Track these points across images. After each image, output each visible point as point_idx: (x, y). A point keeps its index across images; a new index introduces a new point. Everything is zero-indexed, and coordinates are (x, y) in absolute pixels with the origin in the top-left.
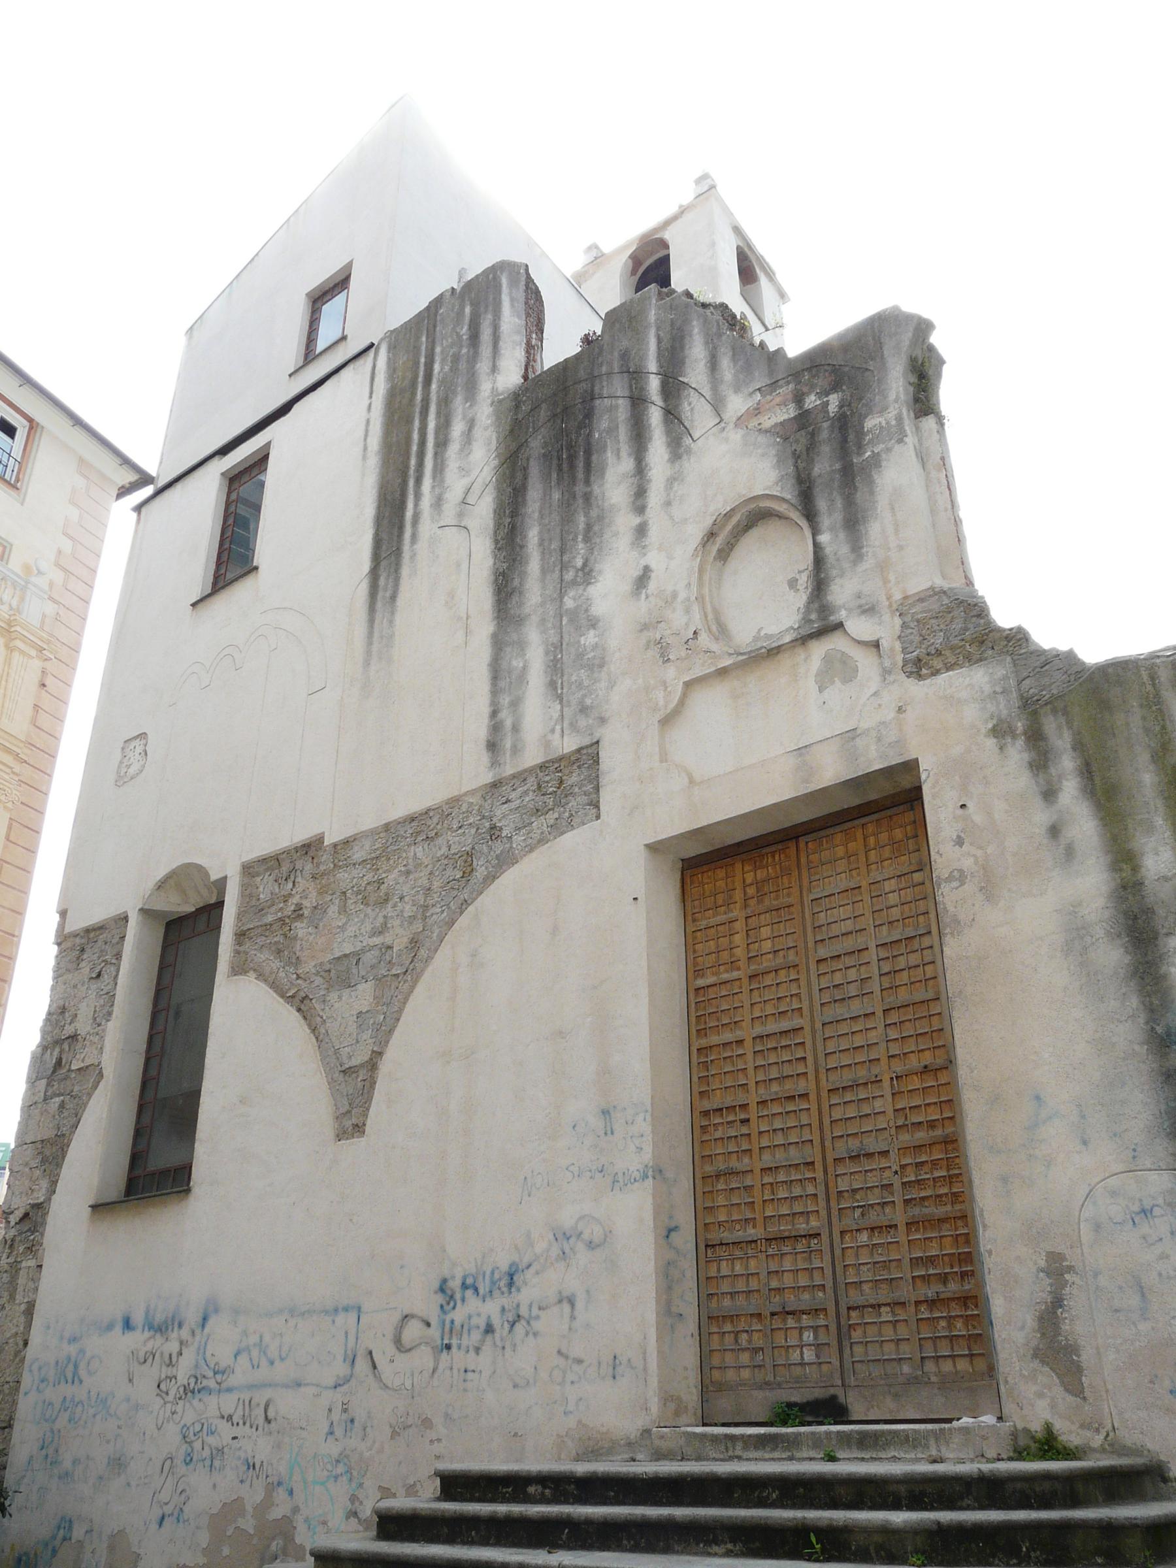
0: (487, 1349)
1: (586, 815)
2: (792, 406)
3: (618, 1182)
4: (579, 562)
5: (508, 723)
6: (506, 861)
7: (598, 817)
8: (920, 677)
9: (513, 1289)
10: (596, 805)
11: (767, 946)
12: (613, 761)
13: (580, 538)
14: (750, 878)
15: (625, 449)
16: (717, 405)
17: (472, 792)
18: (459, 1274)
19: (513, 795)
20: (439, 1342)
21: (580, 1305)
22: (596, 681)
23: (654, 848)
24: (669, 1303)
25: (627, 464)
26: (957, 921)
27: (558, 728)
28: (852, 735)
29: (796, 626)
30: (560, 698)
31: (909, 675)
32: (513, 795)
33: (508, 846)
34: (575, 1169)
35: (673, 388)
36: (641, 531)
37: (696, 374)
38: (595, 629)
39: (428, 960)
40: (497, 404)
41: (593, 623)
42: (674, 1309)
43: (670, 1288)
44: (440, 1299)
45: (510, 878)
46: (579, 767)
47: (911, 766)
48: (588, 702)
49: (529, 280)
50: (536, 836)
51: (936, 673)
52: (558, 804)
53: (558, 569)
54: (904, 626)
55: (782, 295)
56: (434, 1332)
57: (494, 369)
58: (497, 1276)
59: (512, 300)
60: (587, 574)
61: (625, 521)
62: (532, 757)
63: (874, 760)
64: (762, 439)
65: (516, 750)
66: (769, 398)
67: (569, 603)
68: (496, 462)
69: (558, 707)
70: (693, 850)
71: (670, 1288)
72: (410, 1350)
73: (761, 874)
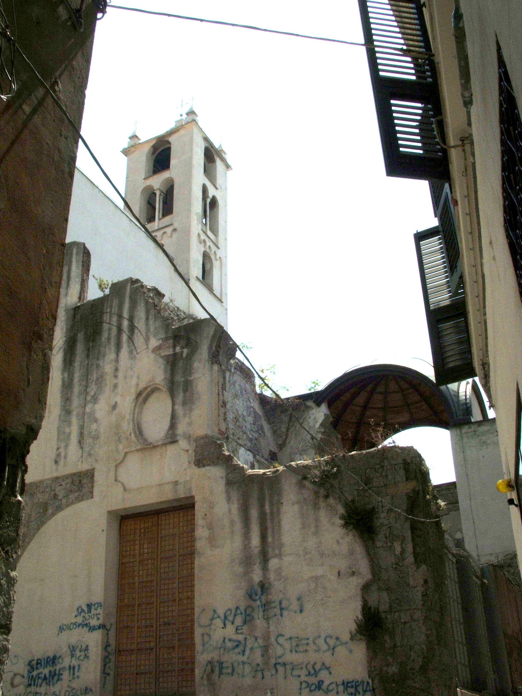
0: (44, 684)
1: (88, 496)
2: (172, 349)
3: (92, 629)
4: (92, 393)
5: (63, 454)
6: (59, 508)
7: (92, 497)
8: (199, 467)
9: (54, 665)
10: (92, 493)
11: (146, 551)
12: (99, 477)
13: (94, 383)
14: (142, 526)
15: (113, 349)
16: (147, 339)
17: (48, 479)
18: (36, 658)
19: (63, 483)
20: (27, 683)
21: (76, 670)
22: (96, 444)
23: (109, 512)
24: (104, 669)
25: (113, 356)
26: (199, 553)
27: (81, 460)
28: (176, 483)
29: (163, 439)
30: (82, 448)
31: (196, 465)
32: (63, 483)
33: (60, 503)
34: (77, 624)
35: (132, 328)
36: (115, 386)
37: (140, 324)
38: (96, 422)
39: (29, 543)
40: (67, 310)
41: (96, 421)
42: (106, 671)
43: (105, 665)
44: (29, 668)
45: (60, 515)
46: (87, 477)
47: (193, 497)
48: (92, 452)
49: (85, 248)
50: (71, 500)
51: (204, 466)
52: (79, 490)
53: (85, 393)
54: (197, 446)
55: (228, 167)
56: (26, 681)
57: (66, 295)
58: (49, 660)
59: (77, 261)
60: (95, 399)
61: (109, 380)
62: (69, 470)
63: (182, 494)
64: (161, 360)
65: (65, 465)
66: (164, 343)
67: (88, 409)
68: (65, 339)
69: (81, 452)
70: (124, 514)
71: (105, 665)
72: (16, 686)
73: (146, 525)
